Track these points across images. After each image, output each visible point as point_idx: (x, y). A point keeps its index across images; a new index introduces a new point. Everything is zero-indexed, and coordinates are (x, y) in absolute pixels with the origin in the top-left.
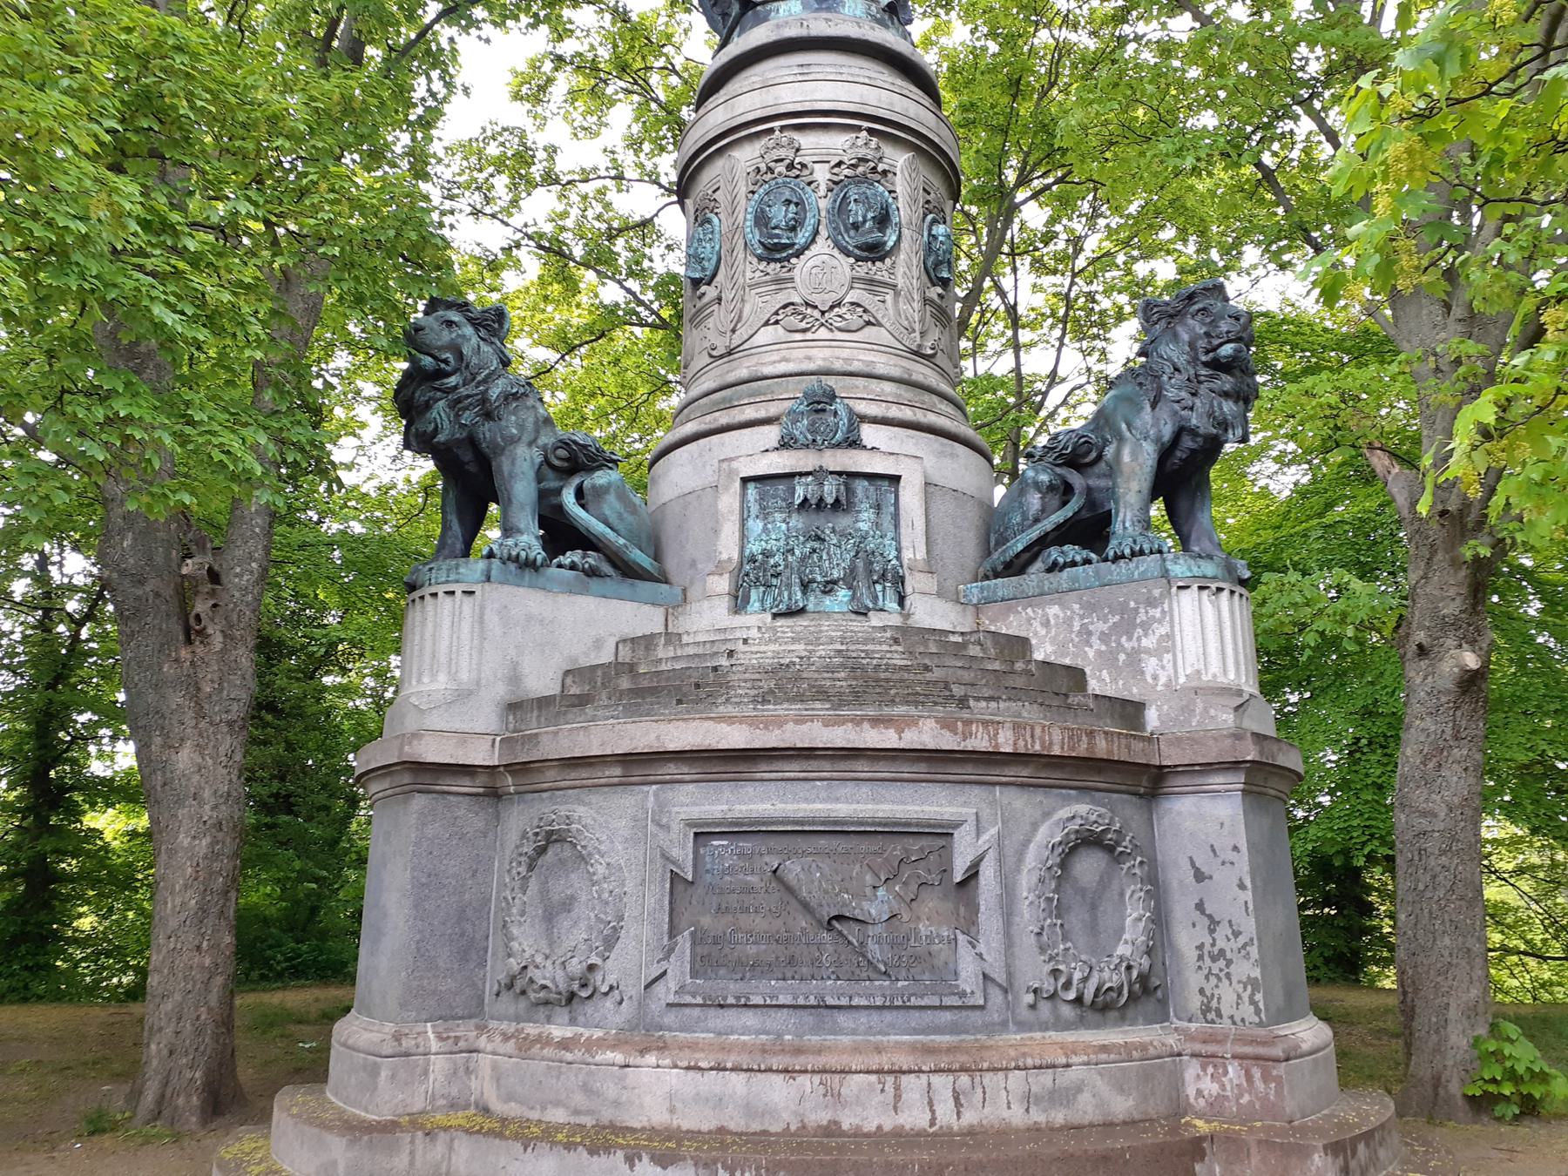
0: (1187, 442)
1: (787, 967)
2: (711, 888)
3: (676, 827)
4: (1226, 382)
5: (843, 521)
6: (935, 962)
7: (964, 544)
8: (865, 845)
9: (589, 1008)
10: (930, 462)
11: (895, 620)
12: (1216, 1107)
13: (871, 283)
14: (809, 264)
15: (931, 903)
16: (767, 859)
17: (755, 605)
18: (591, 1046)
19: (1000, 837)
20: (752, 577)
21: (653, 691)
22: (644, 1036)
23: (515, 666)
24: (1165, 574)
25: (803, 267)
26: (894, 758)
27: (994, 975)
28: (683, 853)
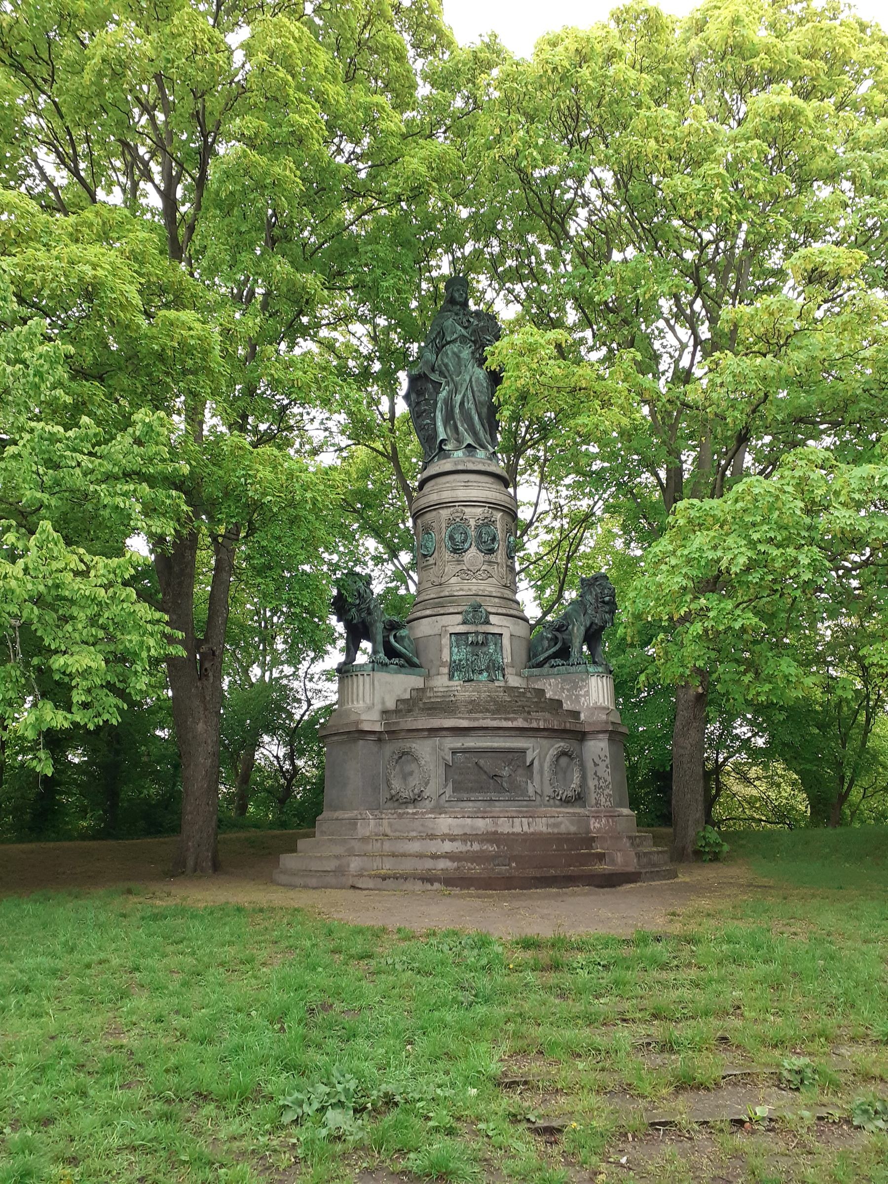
0: (594, 627)
1: (481, 789)
4: (607, 608)
5: (485, 649)
7: (522, 655)
8: (501, 755)
9: (420, 803)
11: (502, 684)
12: (599, 830)
13: (490, 563)
15: (520, 771)
18: (422, 813)
19: (539, 753)
20: (455, 668)
21: (435, 709)
22: (439, 810)
23: (383, 699)
24: (587, 671)
28: (449, 757)
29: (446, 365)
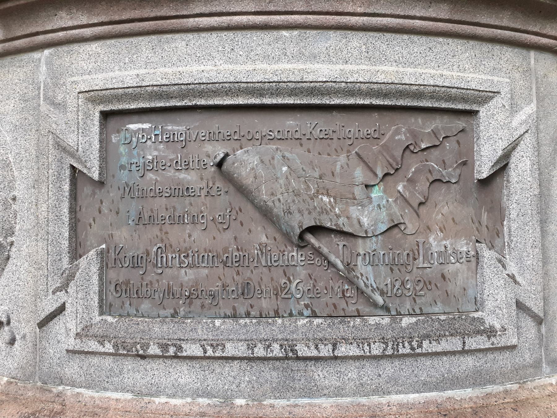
1: (242, 299)
2: (129, 190)
3: (72, 102)
6: (451, 287)
8: (354, 126)
15: (446, 206)
16: (209, 148)
27: (529, 303)
28: (86, 140)
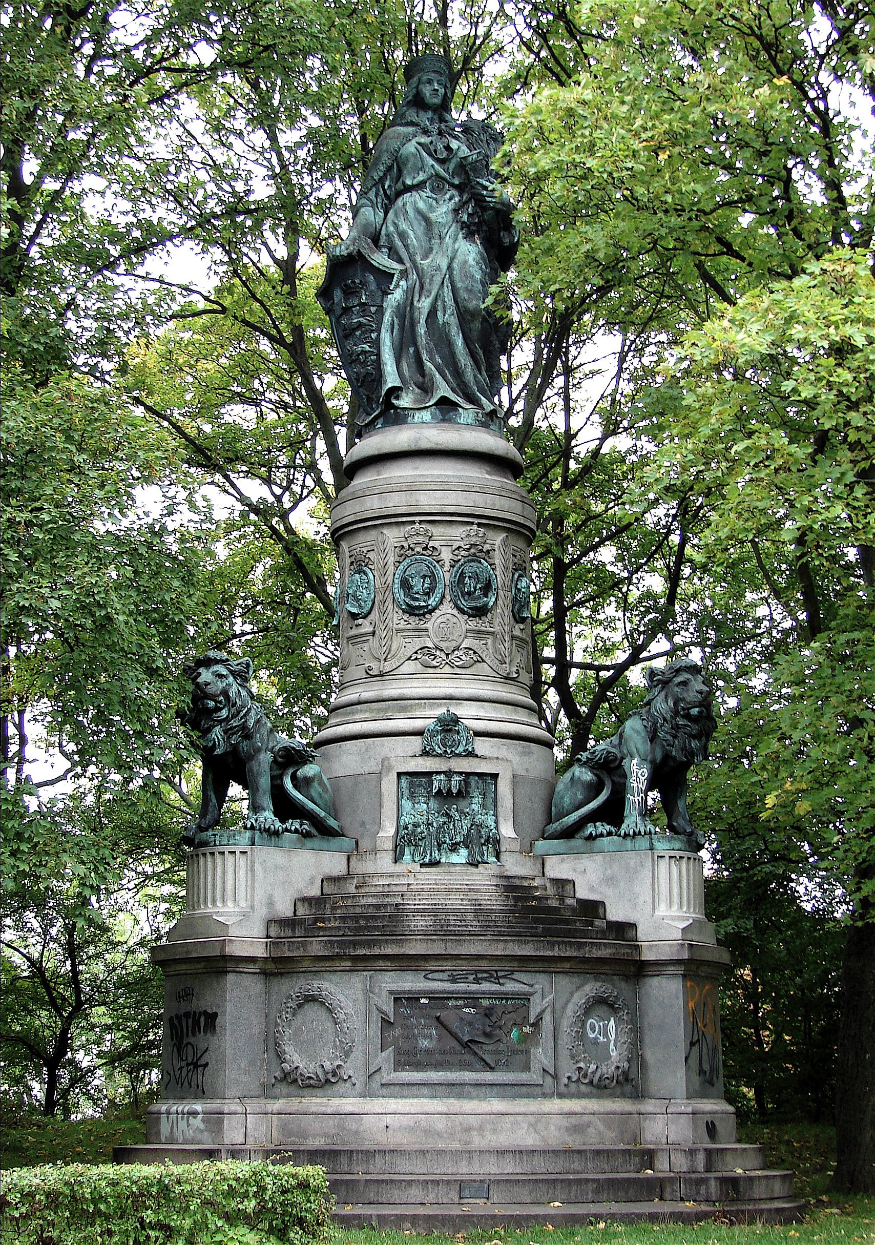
5: (463, 804)
9: (336, 1088)
10: (516, 760)
13: (479, 634)
14: (439, 621)
17: (407, 857)
19: (553, 1004)
25: (433, 622)
26: (501, 960)
29: (403, 236)
